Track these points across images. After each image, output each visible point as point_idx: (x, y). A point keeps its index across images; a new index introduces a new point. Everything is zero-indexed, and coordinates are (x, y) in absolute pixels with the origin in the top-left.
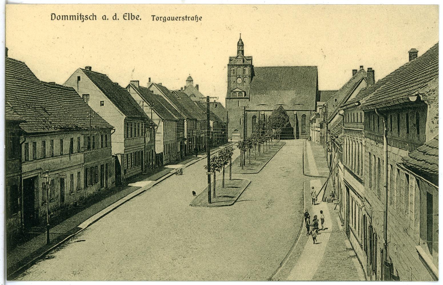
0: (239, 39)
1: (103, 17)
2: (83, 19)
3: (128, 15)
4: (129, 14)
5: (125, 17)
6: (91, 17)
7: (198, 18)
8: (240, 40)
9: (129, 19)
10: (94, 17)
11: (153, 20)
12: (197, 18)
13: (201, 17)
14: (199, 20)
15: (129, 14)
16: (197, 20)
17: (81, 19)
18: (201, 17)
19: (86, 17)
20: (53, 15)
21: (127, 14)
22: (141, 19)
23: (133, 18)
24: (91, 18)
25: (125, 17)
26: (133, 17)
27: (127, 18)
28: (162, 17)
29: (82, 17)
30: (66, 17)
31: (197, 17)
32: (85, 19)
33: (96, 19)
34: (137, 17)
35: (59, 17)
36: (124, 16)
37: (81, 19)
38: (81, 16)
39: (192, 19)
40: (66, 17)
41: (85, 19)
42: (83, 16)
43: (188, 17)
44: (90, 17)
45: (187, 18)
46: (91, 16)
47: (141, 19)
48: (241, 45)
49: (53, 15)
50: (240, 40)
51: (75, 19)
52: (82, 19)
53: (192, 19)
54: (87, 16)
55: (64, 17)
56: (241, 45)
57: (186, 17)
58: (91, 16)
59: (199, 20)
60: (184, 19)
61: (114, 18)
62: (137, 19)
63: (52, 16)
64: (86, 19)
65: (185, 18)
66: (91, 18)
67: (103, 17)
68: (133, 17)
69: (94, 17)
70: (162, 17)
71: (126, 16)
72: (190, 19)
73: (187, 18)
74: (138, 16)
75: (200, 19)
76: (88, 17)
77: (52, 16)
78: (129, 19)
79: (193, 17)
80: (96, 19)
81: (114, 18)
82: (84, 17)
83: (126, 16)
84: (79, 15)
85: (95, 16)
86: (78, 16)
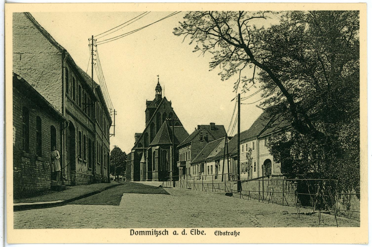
0: (157, 83)
1: (182, 232)
2: (157, 234)
3: (217, 232)
4: (218, 231)
5: (192, 232)
6: (163, 232)
7: (237, 233)
8: (159, 83)
9: (195, 234)
10: (166, 232)
11: (209, 63)
12: (235, 233)
13: (239, 232)
14: (237, 234)
15: (218, 231)
16: (235, 234)
17: (155, 234)
18: (239, 232)
19: (159, 232)
20: (132, 231)
21: (217, 231)
22: (205, 234)
23: (199, 233)
24: (164, 233)
25: (192, 232)
26: (221, 234)
27: (217, 234)
28: (230, 232)
29: (156, 232)
30: (149, 232)
31: (236, 233)
32: (159, 234)
33: (168, 234)
34: (202, 232)
35: (137, 233)
36: (191, 231)
37: (235, 235)
38: (155, 231)
39: (232, 234)
40: (143, 232)
41: (159, 234)
42: (157, 232)
43: (229, 233)
44: (163, 232)
45: (228, 233)
46: (164, 231)
47: (205, 234)
48: (159, 88)
49: (132, 231)
50: (159, 84)
51: (150, 234)
52: (156, 234)
53: (232, 234)
54: (161, 231)
55: (147, 232)
56: (159, 88)
57: (227, 232)
58: (164, 231)
59: (237, 234)
60: (225, 234)
61: (183, 233)
62: (202, 234)
63: (131, 231)
64: (160, 234)
65: (226, 233)
66: (164, 233)
67: (182, 232)
68: (221, 234)
69: (166, 232)
70: (230, 232)
71: (193, 232)
72: (230, 234)
73: (228, 233)
74: (203, 231)
75: (238, 234)
76: (161, 232)
77: (131, 231)
78: (195, 234)
79: (233, 232)
80: (168, 234)
81: (183, 233)
82: (158, 233)
83: (193, 232)
84: (154, 231)
85: (167, 231)
86: (153, 232)
